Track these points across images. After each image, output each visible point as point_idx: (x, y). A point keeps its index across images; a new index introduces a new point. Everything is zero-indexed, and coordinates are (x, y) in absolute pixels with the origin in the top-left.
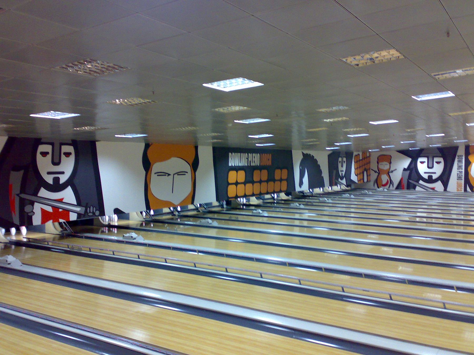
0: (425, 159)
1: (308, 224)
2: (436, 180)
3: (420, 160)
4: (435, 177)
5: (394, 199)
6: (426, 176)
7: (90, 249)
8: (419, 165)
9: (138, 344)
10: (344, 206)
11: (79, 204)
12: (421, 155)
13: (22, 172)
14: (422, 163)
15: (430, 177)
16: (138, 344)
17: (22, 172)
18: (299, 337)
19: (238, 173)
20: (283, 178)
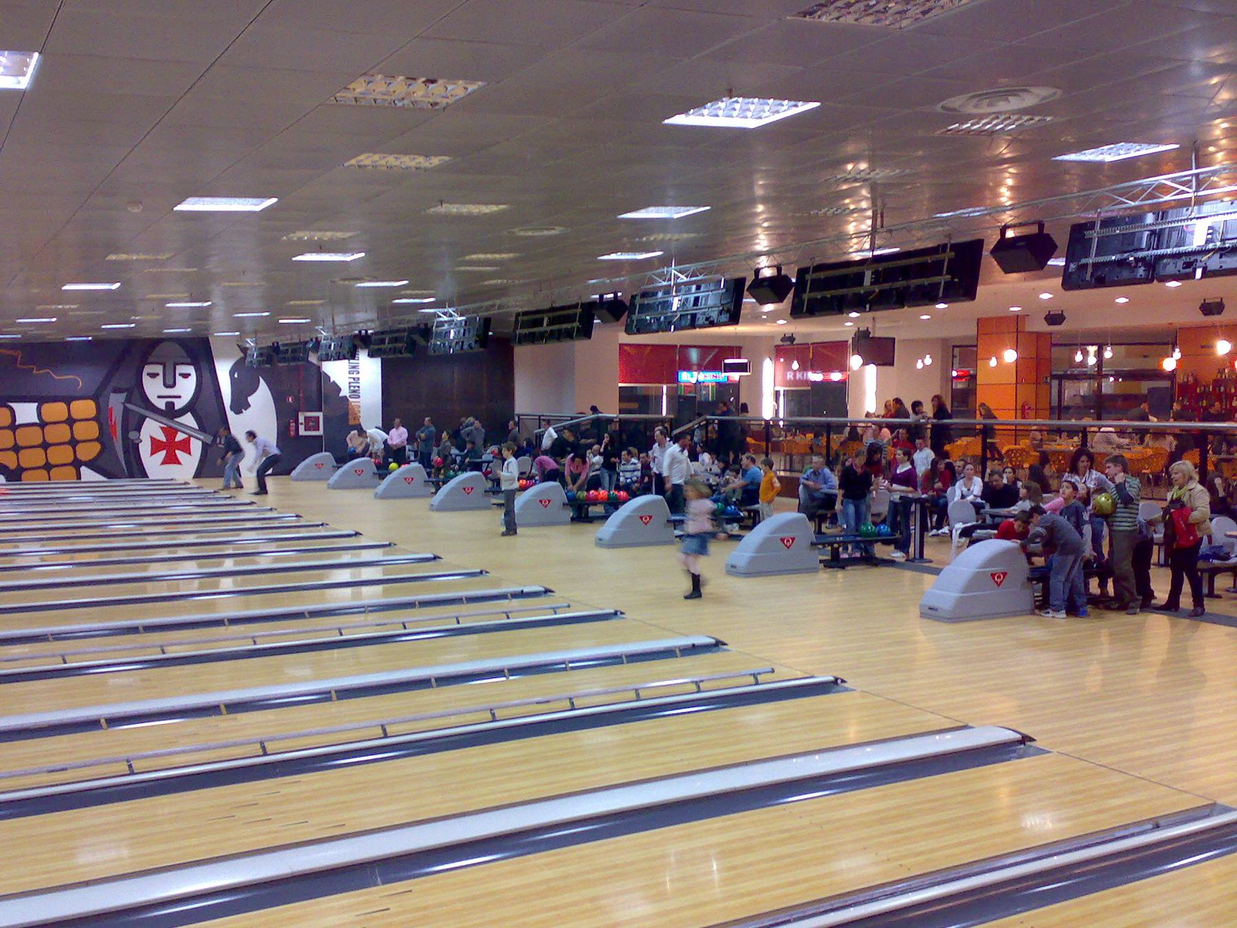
0: (158, 369)
1: (235, 564)
2: (182, 412)
3: (148, 369)
4: (179, 404)
5: (143, 505)
6: (161, 404)
7: (161, 647)
8: (146, 380)
9: (927, 880)
10: (93, 557)
11: (202, 428)
12: (150, 360)
13: (125, 394)
14: (153, 375)
15: (170, 405)
16: (927, 880)
17: (125, 394)
18: (1159, 869)
19: (66, 416)
20: (76, 426)
